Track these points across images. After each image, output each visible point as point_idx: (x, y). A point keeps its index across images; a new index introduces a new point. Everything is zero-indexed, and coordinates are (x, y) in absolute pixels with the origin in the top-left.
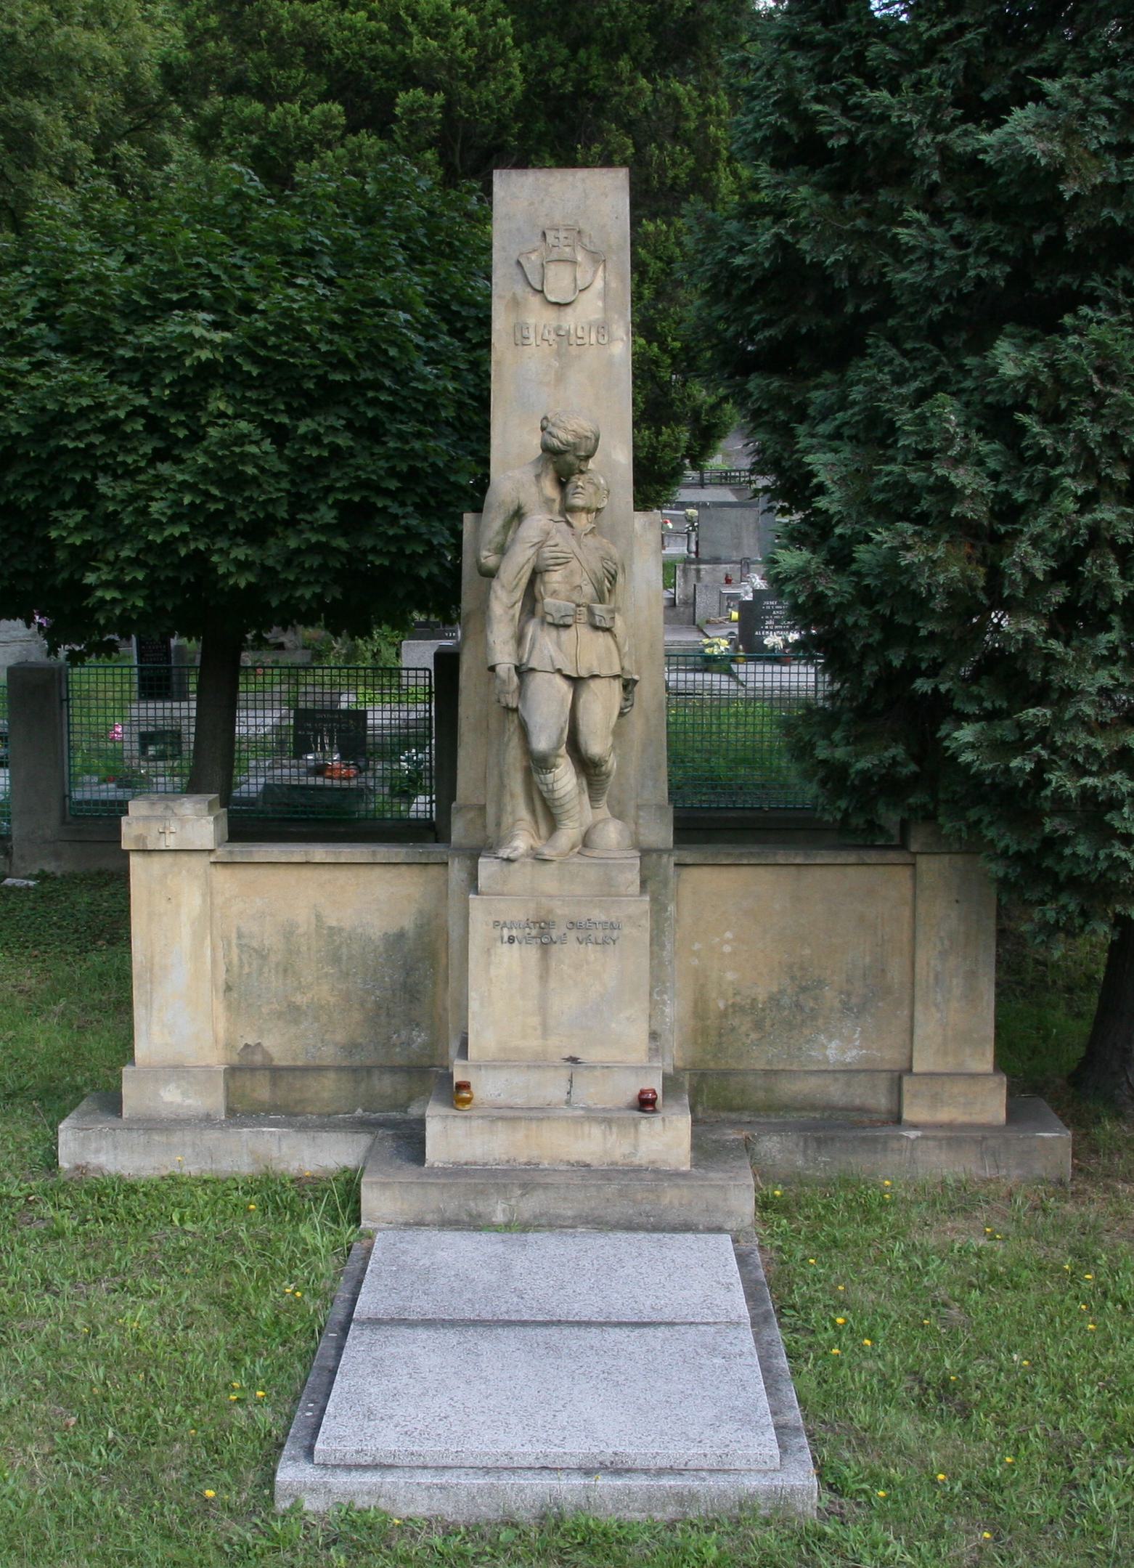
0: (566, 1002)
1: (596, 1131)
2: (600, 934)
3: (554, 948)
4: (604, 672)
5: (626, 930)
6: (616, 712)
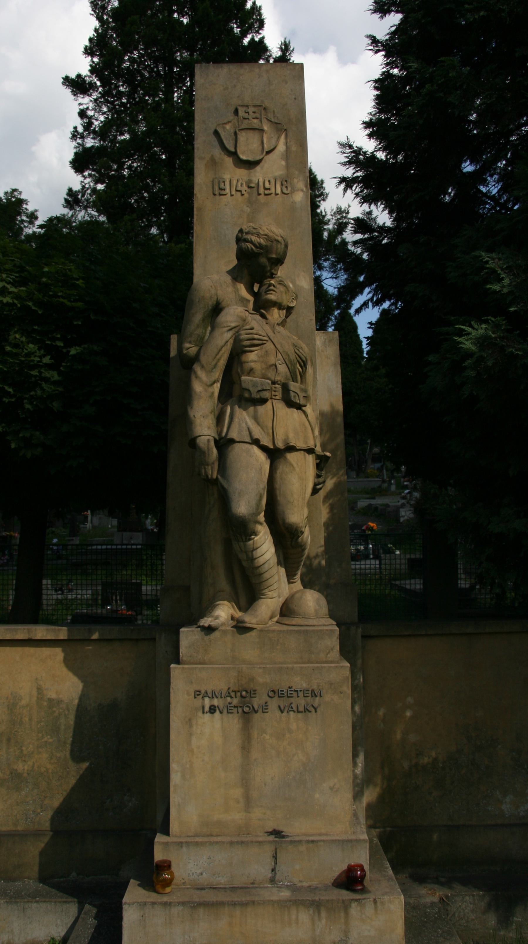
0: (268, 773)
1: (304, 916)
2: (301, 702)
3: (256, 717)
4: (300, 444)
5: (327, 697)
6: (310, 486)
